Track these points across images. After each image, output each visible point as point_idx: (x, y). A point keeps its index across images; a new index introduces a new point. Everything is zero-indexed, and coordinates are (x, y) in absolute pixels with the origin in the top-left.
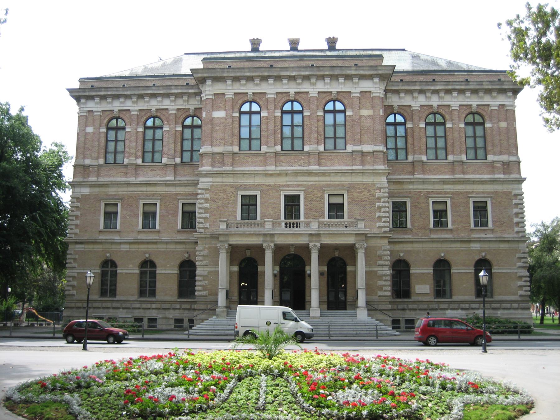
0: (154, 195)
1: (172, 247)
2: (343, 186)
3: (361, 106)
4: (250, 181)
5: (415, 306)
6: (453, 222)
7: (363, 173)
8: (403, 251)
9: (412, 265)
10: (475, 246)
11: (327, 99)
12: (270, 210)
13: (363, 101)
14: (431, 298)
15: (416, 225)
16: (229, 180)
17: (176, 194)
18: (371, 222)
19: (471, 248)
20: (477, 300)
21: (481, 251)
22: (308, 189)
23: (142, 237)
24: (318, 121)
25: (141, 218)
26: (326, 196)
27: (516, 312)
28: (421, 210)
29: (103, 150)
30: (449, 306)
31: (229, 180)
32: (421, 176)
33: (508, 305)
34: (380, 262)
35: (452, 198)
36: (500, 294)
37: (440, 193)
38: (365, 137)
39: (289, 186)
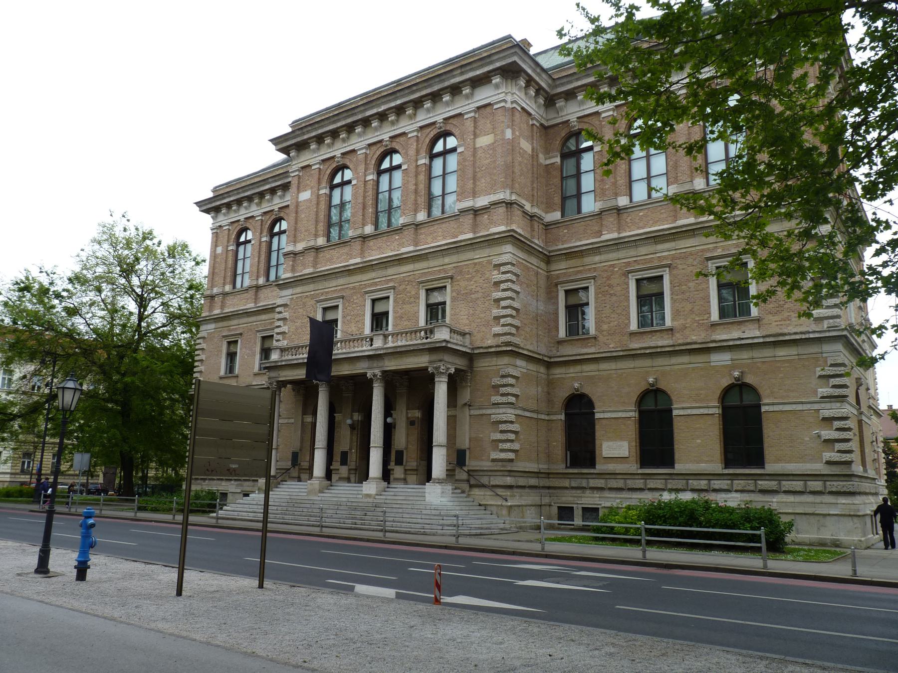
2: (445, 271)
3: (478, 132)
5: (600, 483)
6: (676, 314)
9: (597, 404)
12: (353, 325)
13: (480, 123)
14: (633, 467)
15: (605, 327)
18: (484, 329)
19: (712, 364)
20: (726, 471)
21: (733, 367)
25: (258, 357)
26: (423, 294)
27: (818, 499)
28: (614, 298)
29: (229, 274)
30: (666, 484)
33: (798, 485)
36: (778, 460)
38: (482, 183)
39: (376, 284)
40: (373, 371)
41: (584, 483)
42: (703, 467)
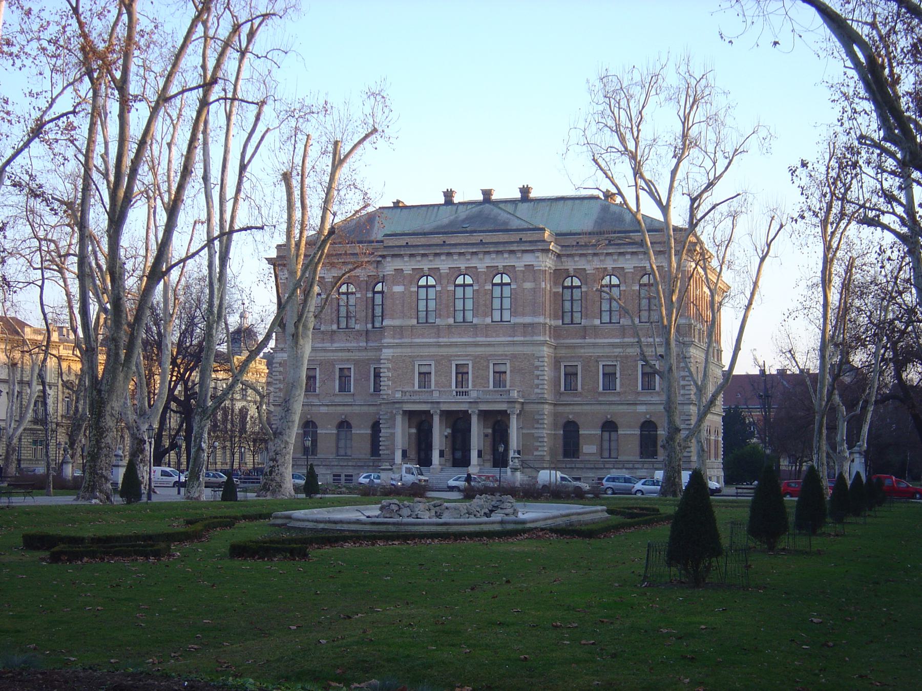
0: (348, 360)
1: (365, 409)
2: (506, 355)
4: (426, 351)
6: (622, 385)
7: (523, 344)
8: (570, 412)
10: (642, 409)
11: (494, 273)
16: (407, 351)
17: (368, 360)
21: (646, 413)
22: (477, 359)
23: (338, 400)
24: (486, 294)
25: (337, 382)
31: (407, 351)
32: (592, 341)
34: (536, 426)
35: (621, 362)
37: (610, 357)
39: (459, 356)
40: (473, 410)
41: (573, 466)
42: (631, 458)
